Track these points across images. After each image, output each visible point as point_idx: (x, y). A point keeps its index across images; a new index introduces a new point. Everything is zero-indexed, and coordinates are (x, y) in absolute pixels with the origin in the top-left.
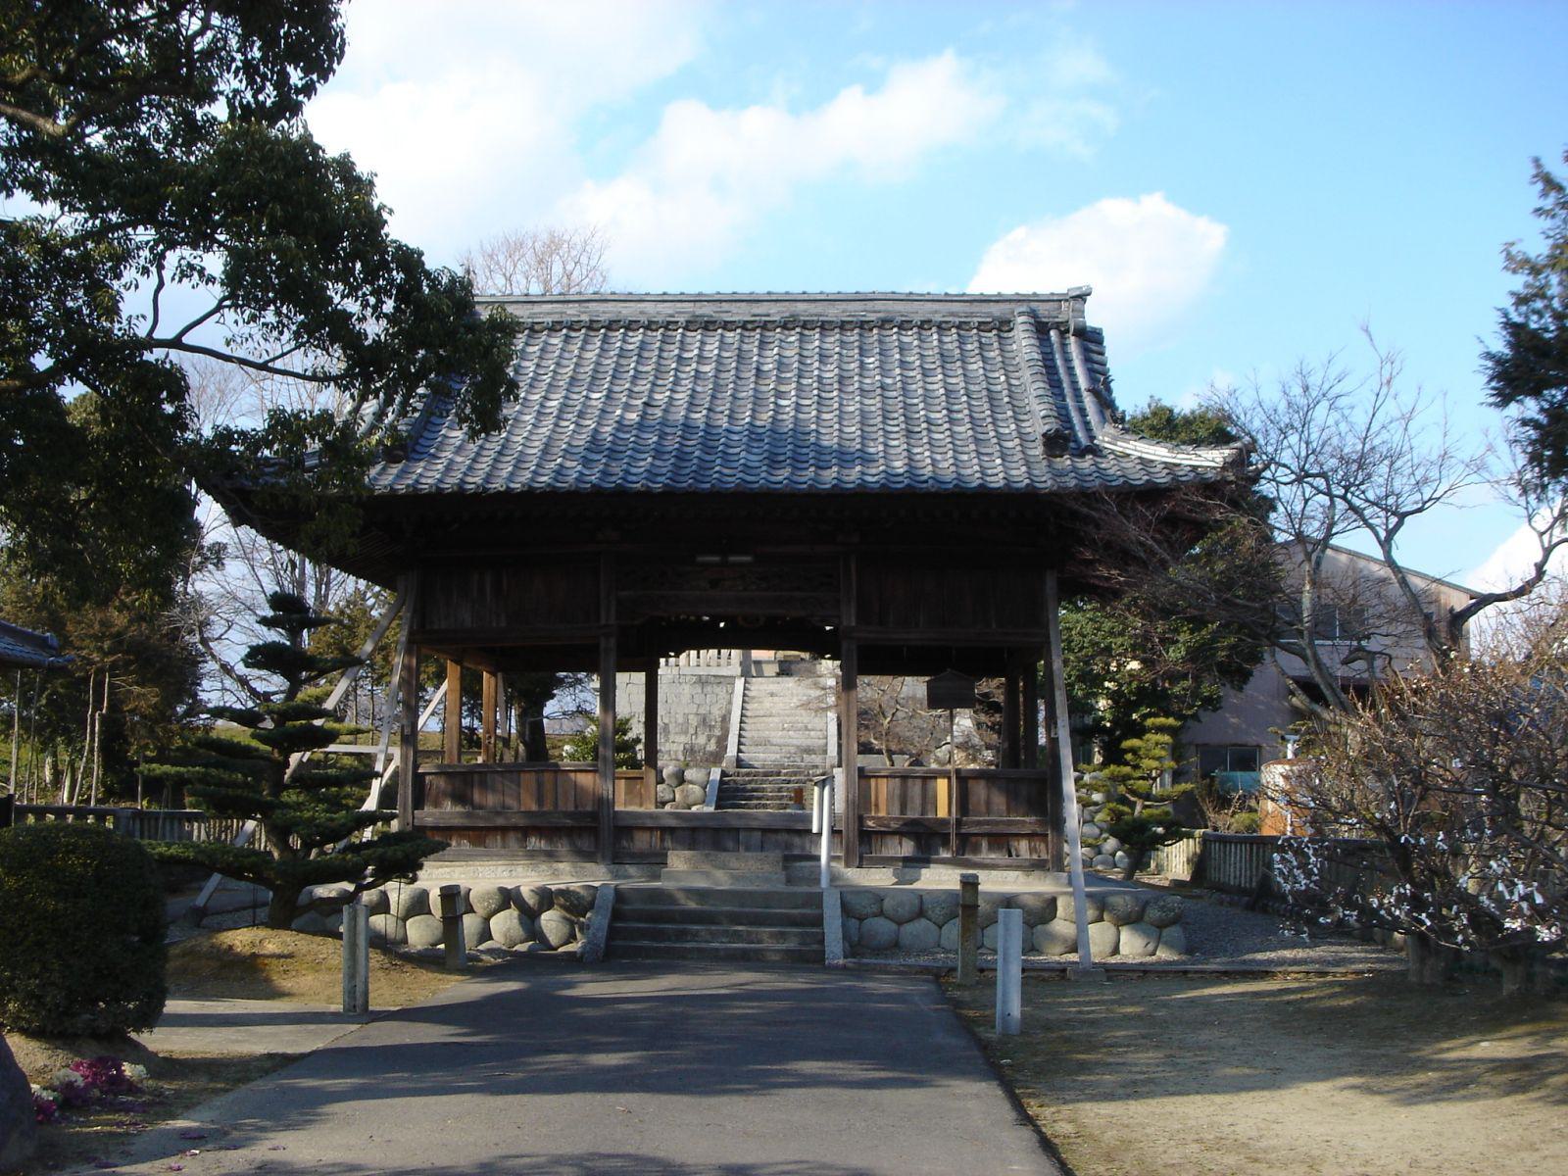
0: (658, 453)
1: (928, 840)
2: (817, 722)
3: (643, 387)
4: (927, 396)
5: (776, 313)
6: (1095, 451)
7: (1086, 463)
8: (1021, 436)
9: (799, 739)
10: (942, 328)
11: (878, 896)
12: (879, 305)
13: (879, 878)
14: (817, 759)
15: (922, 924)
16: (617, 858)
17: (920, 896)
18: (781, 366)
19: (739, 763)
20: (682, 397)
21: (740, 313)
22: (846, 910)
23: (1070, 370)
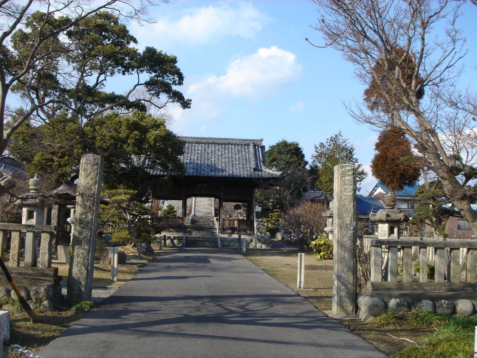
0: (193, 169)
1: (234, 230)
2: (210, 207)
3: (189, 155)
4: (235, 159)
5: (210, 141)
6: (261, 171)
7: (259, 173)
8: (250, 167)
9: (206, 211)
10: (238, 145)
11: (226, 238)
12: (228, 140)
13: (226, 236)
14: (210, 215)
15: (232, 243)
16: (184, 232)
17: (232, 239)
18: (212, 152)
19: (195, 215)
20: (196, 157)
21: (204, 141)
22: (221, 240)
23: (259, 154)
